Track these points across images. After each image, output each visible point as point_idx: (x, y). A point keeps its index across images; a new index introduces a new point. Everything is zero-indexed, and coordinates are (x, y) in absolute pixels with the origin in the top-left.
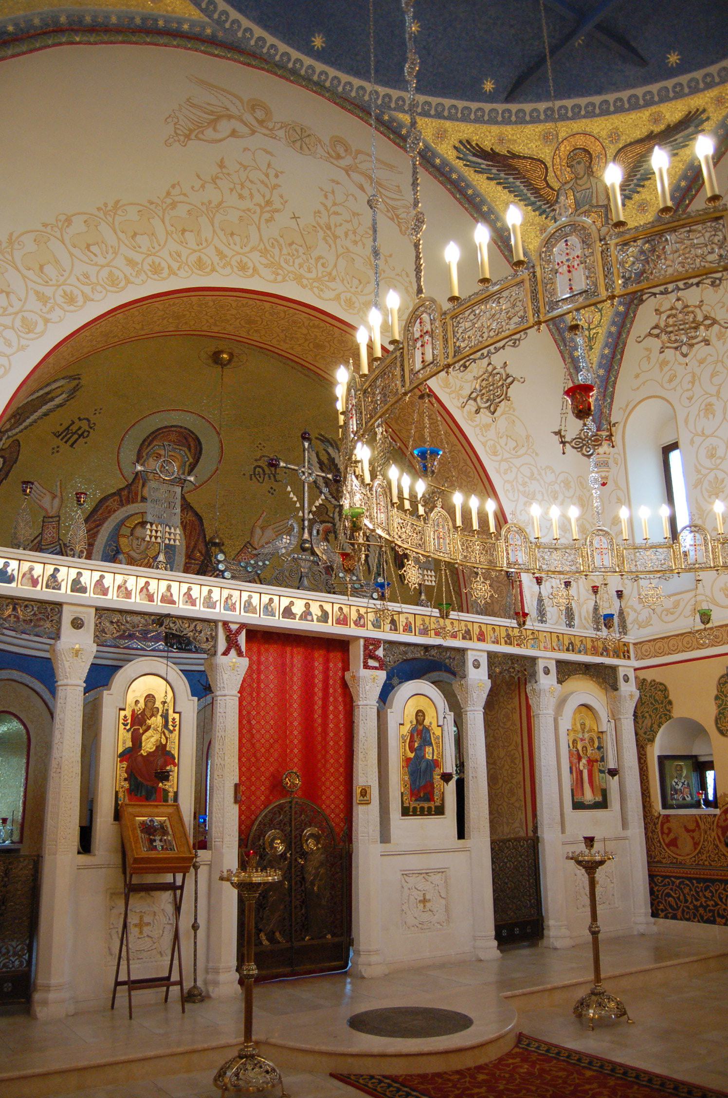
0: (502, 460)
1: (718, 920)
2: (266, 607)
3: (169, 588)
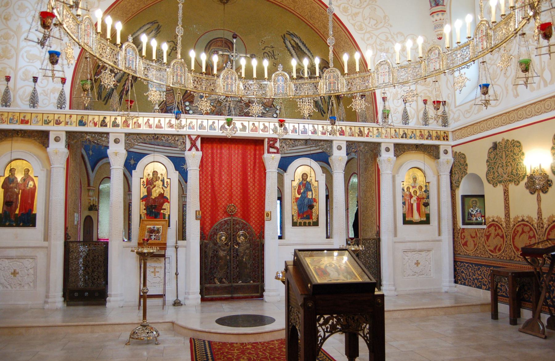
0: (366, 32)
1: (483, 286)
2: (211, 126)
3: (159, 121)
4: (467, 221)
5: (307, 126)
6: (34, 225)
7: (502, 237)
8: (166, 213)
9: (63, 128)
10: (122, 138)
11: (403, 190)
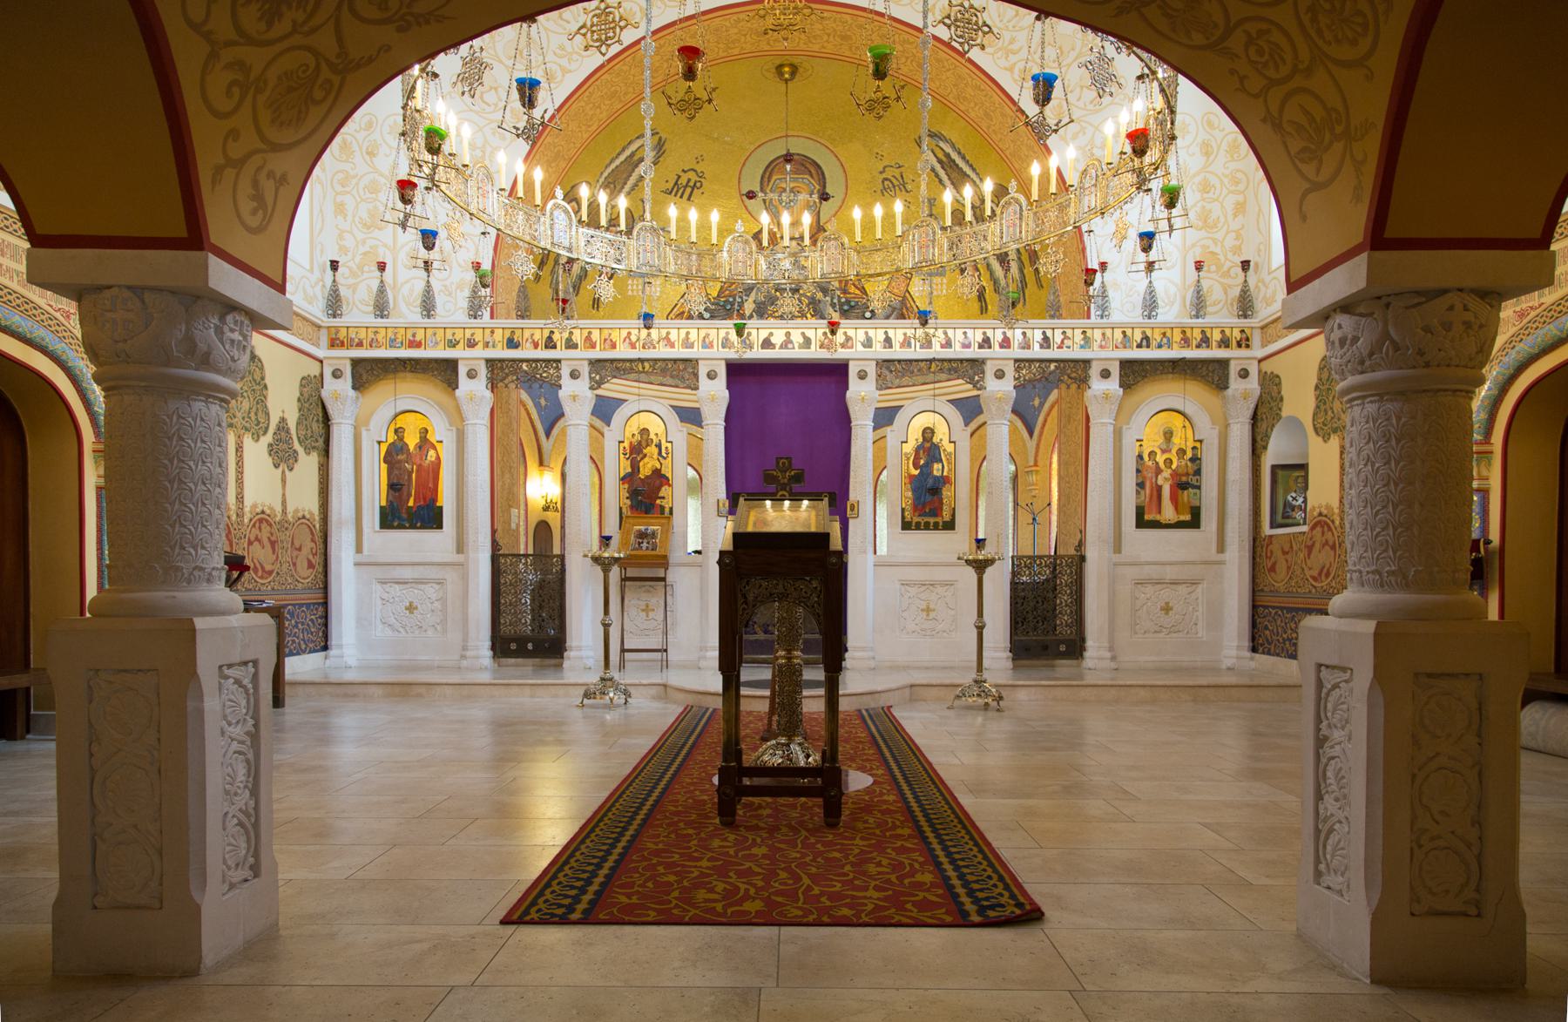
4: (1279, 519)
5: (970, 333)
6: (440, 526)
7: (1333, 547)
8: (667, 504)
9: (480, 352)
10: (585, 369)
11: (1140, 457)
